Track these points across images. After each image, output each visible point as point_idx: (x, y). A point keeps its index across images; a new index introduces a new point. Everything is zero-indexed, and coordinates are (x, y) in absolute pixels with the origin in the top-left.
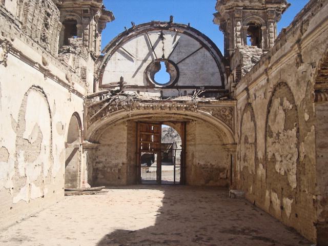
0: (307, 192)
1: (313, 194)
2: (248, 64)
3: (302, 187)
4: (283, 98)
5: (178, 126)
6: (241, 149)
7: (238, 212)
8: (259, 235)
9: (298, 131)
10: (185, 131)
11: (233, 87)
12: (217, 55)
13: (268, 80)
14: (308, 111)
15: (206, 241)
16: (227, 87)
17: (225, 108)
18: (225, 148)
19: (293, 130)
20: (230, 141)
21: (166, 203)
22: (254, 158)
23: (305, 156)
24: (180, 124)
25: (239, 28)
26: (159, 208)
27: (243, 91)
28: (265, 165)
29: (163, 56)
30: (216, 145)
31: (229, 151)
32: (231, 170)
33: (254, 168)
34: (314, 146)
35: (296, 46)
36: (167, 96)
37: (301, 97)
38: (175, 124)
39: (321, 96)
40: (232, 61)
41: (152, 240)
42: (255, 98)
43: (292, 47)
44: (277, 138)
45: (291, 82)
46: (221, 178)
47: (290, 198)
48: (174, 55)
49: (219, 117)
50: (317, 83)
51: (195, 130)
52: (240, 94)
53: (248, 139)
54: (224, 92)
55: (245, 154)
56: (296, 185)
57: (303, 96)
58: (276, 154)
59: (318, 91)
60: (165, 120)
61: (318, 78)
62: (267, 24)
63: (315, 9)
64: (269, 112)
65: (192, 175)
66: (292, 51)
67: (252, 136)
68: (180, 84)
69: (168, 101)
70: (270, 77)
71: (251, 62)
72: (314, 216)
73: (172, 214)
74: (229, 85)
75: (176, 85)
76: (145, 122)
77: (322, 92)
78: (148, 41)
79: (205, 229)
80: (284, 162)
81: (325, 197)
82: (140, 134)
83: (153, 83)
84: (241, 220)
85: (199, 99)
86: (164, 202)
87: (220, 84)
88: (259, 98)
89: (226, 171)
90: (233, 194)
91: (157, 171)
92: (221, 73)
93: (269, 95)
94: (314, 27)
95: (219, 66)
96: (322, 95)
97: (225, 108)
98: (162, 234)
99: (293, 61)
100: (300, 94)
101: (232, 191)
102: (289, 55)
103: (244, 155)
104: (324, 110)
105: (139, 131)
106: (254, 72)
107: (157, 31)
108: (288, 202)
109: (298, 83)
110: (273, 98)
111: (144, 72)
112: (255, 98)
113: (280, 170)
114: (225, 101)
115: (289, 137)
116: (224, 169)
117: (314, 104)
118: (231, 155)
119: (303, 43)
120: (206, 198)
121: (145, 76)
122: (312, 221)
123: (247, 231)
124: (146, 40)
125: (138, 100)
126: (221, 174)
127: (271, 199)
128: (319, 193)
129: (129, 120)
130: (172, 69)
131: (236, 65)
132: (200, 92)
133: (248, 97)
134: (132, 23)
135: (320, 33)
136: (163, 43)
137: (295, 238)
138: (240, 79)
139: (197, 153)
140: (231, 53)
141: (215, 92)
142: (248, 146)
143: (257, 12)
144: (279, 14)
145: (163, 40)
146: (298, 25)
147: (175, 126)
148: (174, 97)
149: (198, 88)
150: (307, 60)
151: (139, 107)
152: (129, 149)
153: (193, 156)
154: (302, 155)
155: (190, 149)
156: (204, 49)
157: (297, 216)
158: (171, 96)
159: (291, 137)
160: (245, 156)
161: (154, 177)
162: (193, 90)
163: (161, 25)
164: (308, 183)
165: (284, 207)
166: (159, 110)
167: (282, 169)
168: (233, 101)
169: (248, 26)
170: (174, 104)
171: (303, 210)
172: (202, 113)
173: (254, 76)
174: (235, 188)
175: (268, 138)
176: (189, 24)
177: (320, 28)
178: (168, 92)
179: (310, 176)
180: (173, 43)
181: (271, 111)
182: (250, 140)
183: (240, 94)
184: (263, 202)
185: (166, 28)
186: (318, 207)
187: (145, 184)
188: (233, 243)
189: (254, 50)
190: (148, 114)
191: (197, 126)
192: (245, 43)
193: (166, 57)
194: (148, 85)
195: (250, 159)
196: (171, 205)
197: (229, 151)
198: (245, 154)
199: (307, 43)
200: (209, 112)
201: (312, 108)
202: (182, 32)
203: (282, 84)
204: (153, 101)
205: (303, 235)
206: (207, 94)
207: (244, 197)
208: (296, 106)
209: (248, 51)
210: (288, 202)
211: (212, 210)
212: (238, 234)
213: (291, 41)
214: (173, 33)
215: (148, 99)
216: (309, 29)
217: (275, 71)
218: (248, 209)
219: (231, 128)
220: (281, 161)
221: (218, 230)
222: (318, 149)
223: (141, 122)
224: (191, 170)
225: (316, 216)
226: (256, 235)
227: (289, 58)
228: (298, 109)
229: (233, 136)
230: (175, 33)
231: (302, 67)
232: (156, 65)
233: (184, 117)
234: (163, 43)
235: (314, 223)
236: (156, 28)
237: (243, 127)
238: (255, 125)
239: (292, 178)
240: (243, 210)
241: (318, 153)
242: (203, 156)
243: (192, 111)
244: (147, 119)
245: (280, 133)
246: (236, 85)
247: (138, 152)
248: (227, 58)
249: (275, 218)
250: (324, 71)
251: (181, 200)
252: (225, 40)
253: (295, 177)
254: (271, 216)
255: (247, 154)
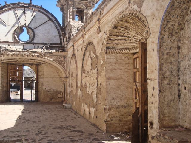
0: (101, 104)
1: (104, 105)
2: (74, 31)
3: (99, 101)
4: (91, 51)
5: (34, 67)
6: (70, 80)
7: (66, 117)
8: (75, 129)
9: (98, 70)
10: (38, 70)
11: (66, 44)
12: (58, 25)
13: (84, 41)
14: (103, 59)
15: (44, 135)
16: (63, 45)
17: (61, 57)
18: (61, 80)
19: (95, 69)
20: (64, 76)
21: (24, 113)
22: (76, 85)
23: (101, 84)
24: (35, 66)
25: (71, 10)
26: (19, 116)
27: (71, 47)
28: (81, 90)
29: (25, 24)
30: (56, 78)
31: (63, 81)
32: (65, 92)
33: (76, 91)
34: (105, 78)
35: (97, 22)
36: (27, 48)
37: (99, 51)
38: (32, 66)
39: (109, 50)
40: (66, 29)
41: (10, 135)
42: (77, 51)
43: (95, 23)
44: (87, 74)
45: (95, 43)
46: (59, 97)
47: (94, 108)
48: (32, 24)
49: (57, 62)
50: (107, 43)
51: (44, 69)
52: (70, 48)
53: (73, 75)
54: (61, 47)
55: (72, 83)
56: (96, 100)
57: (101, 50)
58: (87, 83)
59: (108, 48)
60: (26, 63)
61: (108, 41)
62: (87, 10)
63: (107, 2)
64: (84, 59)
65: (41, 96)
66: (96, 25)
67: (75, 72)
68: (35, 41)
69: (27, 52)
70: (85, 39)
71: (76, 30)
72: (105, 117)
73: (26, 119)
74: (64, 43)
75: (32, 42)
76: (13, 64)
77: (110, 49)
78: (16, 15)
79: (44, 127)
80: (91, 87)
81: (110, 107)
82: (10, 71)
83: (18, 40)
84: (67, 121)
85: (46, 51)
86: (22, 112)
87: (59, 43)
88: (79, 51)
89: (62, 93)
90: (65, 106)
91: (20, 94)
92: (60, 36)
93: (84, 49)
94: (107, 12)
95: (59, 32)
96: (110, 50)
97: (61, 57)
98: (17, 132)
99: (96, 31)
100: (99, 49)
101: (64, 104)
102: (94, 27)
103: (71, 83)
104: (110, 59)
105: (9, 70)
106: (77, 36)
107: (21, 8)
108: (93, 110)
109: (98, 43)
110: (86, 51)
111: (13, 33)
112: (77, 51)
113: (89, 92)
114: (61, 52)
115: (93, 73)
116: (61, 92)
117: (105, 55)
118: (65, 84)
119: (101, 20)
120: (49, 109)
121: (13, 35)
122: (104, 120)
123: (69, 127)
124: (15, 14)
125: (8, 50)
126: (59, 95)
127: (84, 108)
128: (107, 104)
129: (3, 63)
130: (31, 32)
131: (68, 32)
132: (47, 46)
133: (74, 51)
134: (5, 2)
135: (109, 16)
136: (25, 16)
137: (95, 130)
138: (70, 40)
139: (45, 83)
140: (66, 24)
141: (56, 47)
142: (73, 78)
143: (82, 2)
144: (94, 4)
145: (25, 14)
146: (99, 10)
147: (32, 67)
148: (31, 49)
149: (46, 44)
150: (103, 30)
151: (8, 55)
152: (3, 81)
153: (42, 84)
154: (99, 83)
155: (41, 80)
156: (50, 21)
157: (97, 117)
158: (29, 48)
159: (94, 73)
160: (72, 84)
161: (19, 97)
162: (43, 45)
163: (24, 5)
164: (102, 99)
165: (91, 112)
166: (21, 57)
167: (90, 91)
168: (66, 53)
169: (76, 10)
170: (30, 53)
171: (100, 114)
172: (47, 59)
173: (77, 38)
174: (66, 103)
175: (83, 74)
176: (41, 6)
177: (109, 13)
178: (28, 46)
179: (103, 95)
180: (32, 16)
181: (85, 59)
182: (75, 75)
183: (70, 48)
184: (80, 111)
185: (28, 7)
186: (107, 112)
187: (13, 102)
188: (59, 135)
189: (79, 24)
190: (15, 59)
191: (45, 66)
192: (74, 19)
193: (27, 25)
194: (15, 41)
195: (74, 86)
196: (27, 114)
197: (63, 81)
198: (72, 83)
199: (103, 21)
200: (52, 59)
201: (104, 57)
202: (37, 10)
203: (90, 43)
204: (17, 51)
205: (100, 128)
206: (51, 48)
207: (71, 108)
208: (97, 56)
209: (75, 24)
210: (93, 110)
211: (51, 116)
212: (64, 129)
213: (95, 18)
214: (31, 10)
215: (15, 50)
216: (104, 13)
217: (87, 36)
218: (73, 114)
219: (65, 69)
220: (89, 87)
221: (52, 128)
222: (107, 80)
223: (10, 64)
224: (41, 93)
225: (106, 117)
226: (73, 129)
227: (94, 28)
228: (98, 57)
229: (65, 73)
230: (33, 11)
231: (100, 34)
232: (20, 30)
233: (37, 61)
234: (25, 16)
235: (105, 121)
236: (21, 6)
237: (71, 68)
238: (77, 66)
239: (95, 96)
240: (69, 115)
241: (107, 82)
242: (48, 84)
243: (41, 58)
244: (14, 62)
245: (89, 71)
246: (68, 43)
247: (8, 83)
248: (63, 27)
249: (86, 119)
250: (111, 37)
251: (33, 111)
252: (63, 17)
253: (96, 96)
254: (84, 118)
255: (73, 83)
